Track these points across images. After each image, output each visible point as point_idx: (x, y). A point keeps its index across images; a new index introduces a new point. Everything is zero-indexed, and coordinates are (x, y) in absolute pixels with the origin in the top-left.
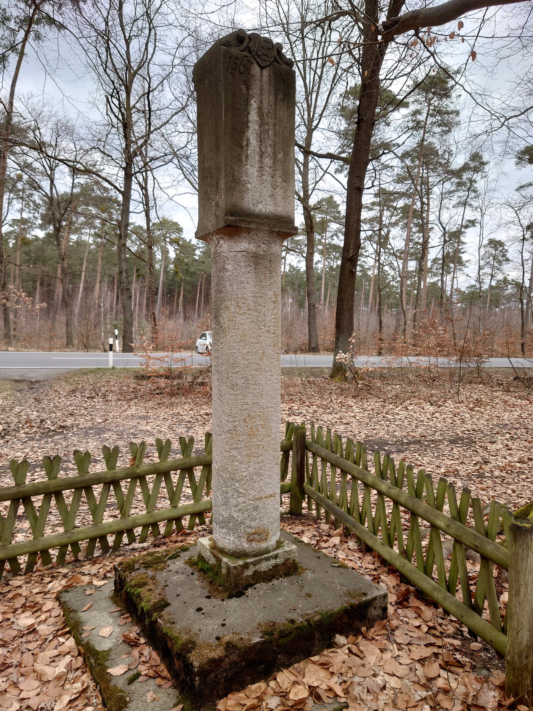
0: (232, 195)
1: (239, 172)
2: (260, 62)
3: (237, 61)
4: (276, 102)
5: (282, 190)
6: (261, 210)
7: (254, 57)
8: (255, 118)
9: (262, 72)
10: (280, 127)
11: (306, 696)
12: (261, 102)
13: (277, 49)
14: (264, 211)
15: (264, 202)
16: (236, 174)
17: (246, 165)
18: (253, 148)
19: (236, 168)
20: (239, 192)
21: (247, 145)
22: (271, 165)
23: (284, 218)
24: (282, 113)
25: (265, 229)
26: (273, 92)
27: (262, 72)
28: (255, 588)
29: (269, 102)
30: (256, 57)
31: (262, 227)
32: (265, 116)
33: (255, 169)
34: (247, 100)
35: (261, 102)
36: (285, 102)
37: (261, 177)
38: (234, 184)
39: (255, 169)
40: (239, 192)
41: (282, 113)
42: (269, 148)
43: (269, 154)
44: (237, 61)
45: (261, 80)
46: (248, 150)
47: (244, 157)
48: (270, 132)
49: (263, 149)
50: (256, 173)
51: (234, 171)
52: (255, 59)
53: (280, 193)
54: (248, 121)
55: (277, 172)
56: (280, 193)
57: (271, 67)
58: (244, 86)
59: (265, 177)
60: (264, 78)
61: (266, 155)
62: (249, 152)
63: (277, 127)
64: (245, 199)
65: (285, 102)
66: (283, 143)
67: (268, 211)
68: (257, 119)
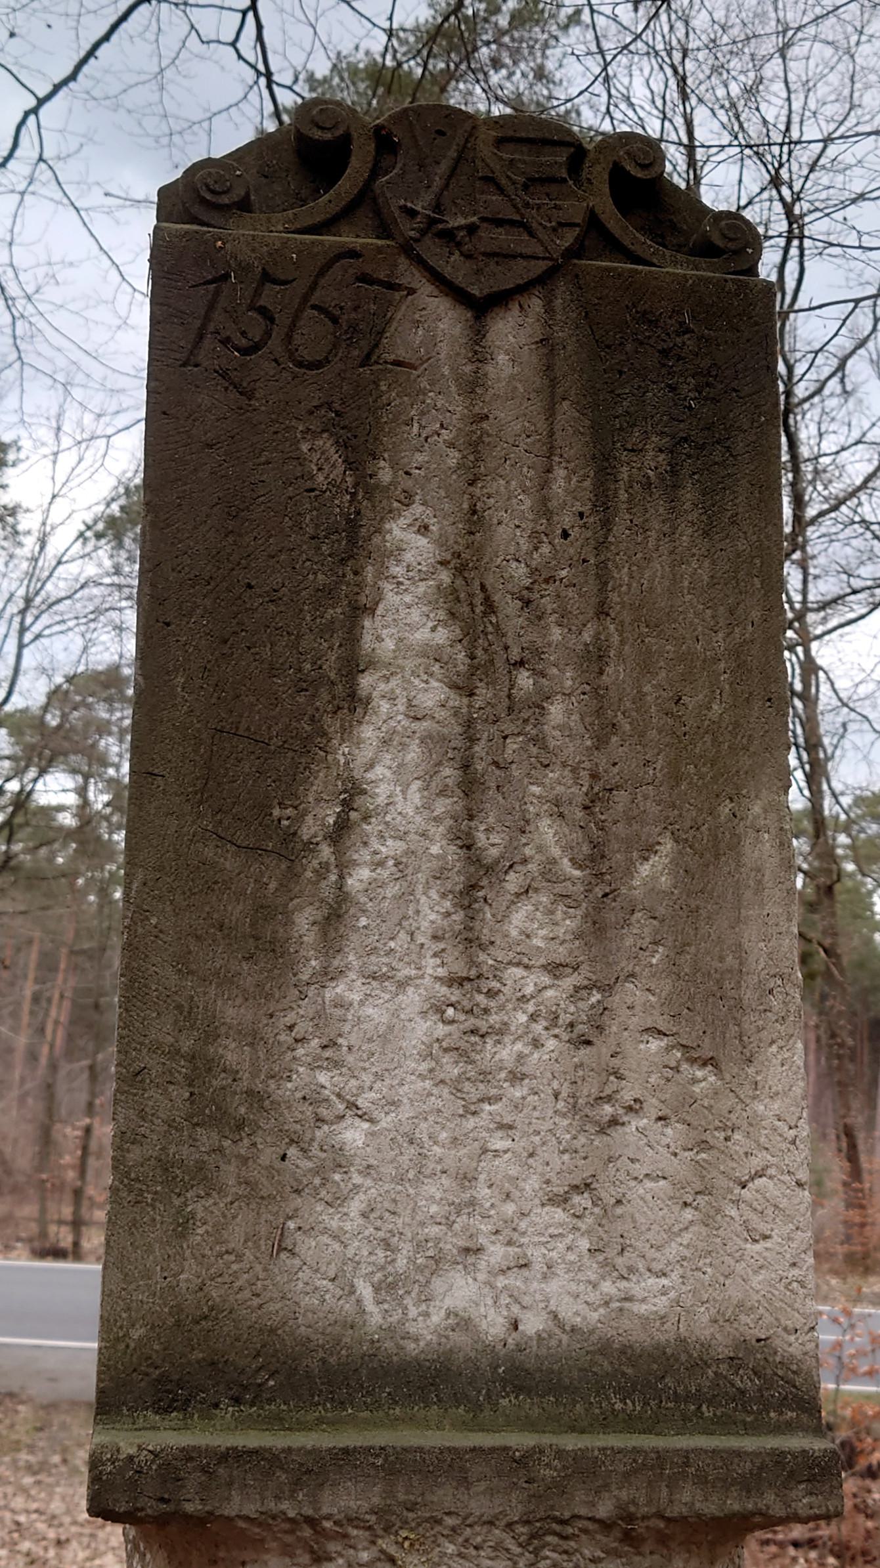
0: (183, 1225)
1: (253, 1038)
2: (454, 267)
3: (269, 297)
4: (603, 502)
5: (672, 1133)
6: (463, 1323)
7: (407, 249)
8: (422, 635)
9: (478, 334)
10: (646, 666)
11: (39, 786)
12: (474, 519)
13: (618, 175)
14: (493, 1325)
15: (497, 1253)
16: (231, 1053)
17: (328, 975)
18: (391, 848)
19: (232, 1013)
20: (252, 1193)
21: (340, 832)
22: (561, 953)
23: (699, 1364)
24: (659, 567)
25: (479, 1505)
26: (573, 446)
27: (478, 334)
28: (151, 56)
29: (544, 509)
30: (431, 250)
31: (444, 1495)
32: (509, 607)
33: (412, 999)
34: (353, 525)
35: (474, 519)
36: (688, 495)
37: (462, 1054)
38: (207, 1138)
39: (412, 999)
40: (252, 1193)
41: (659, 567)
42: (547, 831)
43: (549, 873)
44: (269, 297)
45: (473, 386)
46: (344, 867)
47: (305, 921)
48: (556, 711)
49: (491, 843)
50: (424, 1029)
51: (211, 1036)
52: (421, 263)
53: (655, 1159)
54: (353, 666)
55: (632, 993)
56: (655, 1159)
57: (562, 292)
58: (325, 443)
59: (507, 1052)
60: (502, 366)
61: (513, 882)
62: (359, 878)
63: (615, 673)
64: (307, 1246)
65: (688, 495)
66: (676, 777)
67: (532, 1324)
68: (442, 636)
